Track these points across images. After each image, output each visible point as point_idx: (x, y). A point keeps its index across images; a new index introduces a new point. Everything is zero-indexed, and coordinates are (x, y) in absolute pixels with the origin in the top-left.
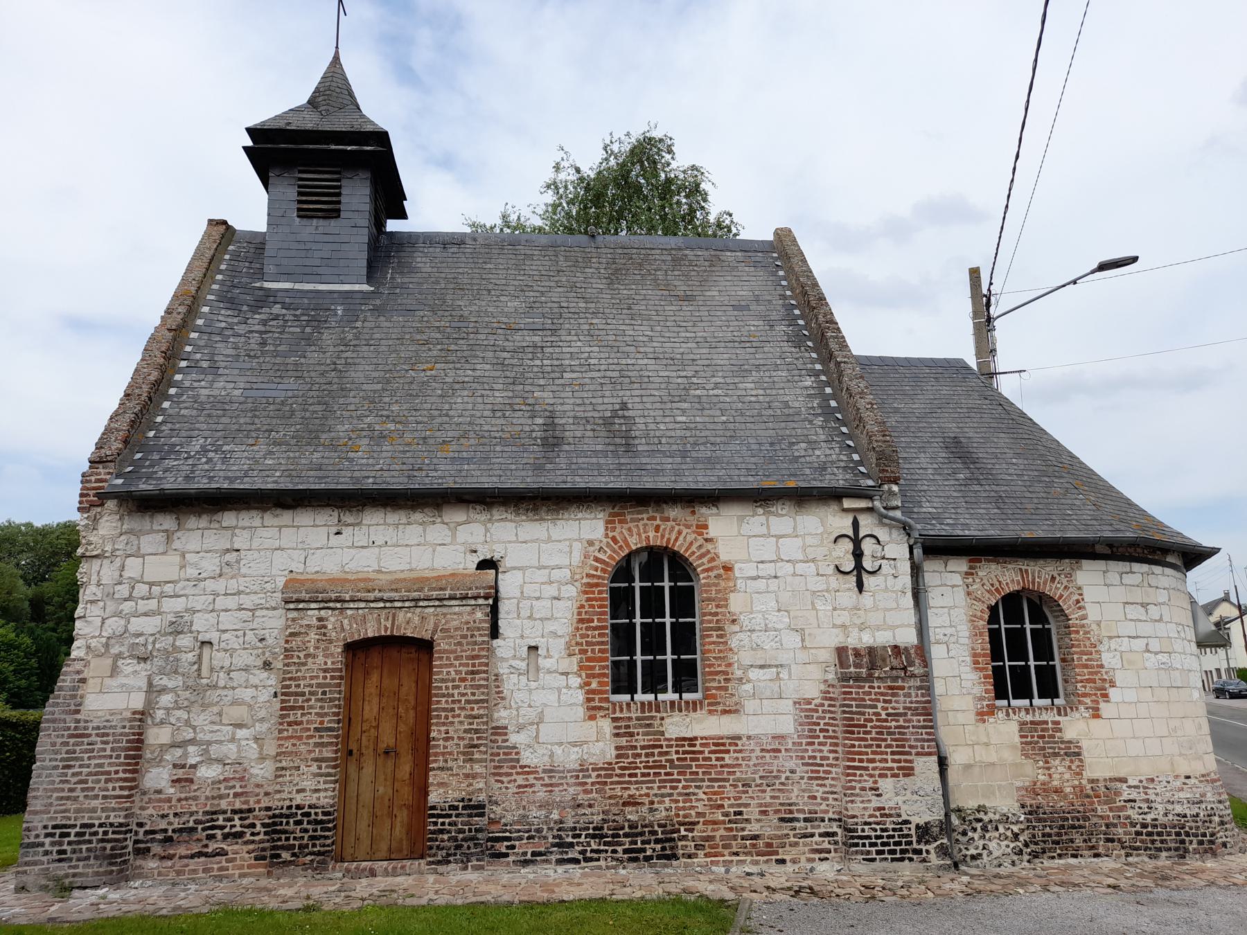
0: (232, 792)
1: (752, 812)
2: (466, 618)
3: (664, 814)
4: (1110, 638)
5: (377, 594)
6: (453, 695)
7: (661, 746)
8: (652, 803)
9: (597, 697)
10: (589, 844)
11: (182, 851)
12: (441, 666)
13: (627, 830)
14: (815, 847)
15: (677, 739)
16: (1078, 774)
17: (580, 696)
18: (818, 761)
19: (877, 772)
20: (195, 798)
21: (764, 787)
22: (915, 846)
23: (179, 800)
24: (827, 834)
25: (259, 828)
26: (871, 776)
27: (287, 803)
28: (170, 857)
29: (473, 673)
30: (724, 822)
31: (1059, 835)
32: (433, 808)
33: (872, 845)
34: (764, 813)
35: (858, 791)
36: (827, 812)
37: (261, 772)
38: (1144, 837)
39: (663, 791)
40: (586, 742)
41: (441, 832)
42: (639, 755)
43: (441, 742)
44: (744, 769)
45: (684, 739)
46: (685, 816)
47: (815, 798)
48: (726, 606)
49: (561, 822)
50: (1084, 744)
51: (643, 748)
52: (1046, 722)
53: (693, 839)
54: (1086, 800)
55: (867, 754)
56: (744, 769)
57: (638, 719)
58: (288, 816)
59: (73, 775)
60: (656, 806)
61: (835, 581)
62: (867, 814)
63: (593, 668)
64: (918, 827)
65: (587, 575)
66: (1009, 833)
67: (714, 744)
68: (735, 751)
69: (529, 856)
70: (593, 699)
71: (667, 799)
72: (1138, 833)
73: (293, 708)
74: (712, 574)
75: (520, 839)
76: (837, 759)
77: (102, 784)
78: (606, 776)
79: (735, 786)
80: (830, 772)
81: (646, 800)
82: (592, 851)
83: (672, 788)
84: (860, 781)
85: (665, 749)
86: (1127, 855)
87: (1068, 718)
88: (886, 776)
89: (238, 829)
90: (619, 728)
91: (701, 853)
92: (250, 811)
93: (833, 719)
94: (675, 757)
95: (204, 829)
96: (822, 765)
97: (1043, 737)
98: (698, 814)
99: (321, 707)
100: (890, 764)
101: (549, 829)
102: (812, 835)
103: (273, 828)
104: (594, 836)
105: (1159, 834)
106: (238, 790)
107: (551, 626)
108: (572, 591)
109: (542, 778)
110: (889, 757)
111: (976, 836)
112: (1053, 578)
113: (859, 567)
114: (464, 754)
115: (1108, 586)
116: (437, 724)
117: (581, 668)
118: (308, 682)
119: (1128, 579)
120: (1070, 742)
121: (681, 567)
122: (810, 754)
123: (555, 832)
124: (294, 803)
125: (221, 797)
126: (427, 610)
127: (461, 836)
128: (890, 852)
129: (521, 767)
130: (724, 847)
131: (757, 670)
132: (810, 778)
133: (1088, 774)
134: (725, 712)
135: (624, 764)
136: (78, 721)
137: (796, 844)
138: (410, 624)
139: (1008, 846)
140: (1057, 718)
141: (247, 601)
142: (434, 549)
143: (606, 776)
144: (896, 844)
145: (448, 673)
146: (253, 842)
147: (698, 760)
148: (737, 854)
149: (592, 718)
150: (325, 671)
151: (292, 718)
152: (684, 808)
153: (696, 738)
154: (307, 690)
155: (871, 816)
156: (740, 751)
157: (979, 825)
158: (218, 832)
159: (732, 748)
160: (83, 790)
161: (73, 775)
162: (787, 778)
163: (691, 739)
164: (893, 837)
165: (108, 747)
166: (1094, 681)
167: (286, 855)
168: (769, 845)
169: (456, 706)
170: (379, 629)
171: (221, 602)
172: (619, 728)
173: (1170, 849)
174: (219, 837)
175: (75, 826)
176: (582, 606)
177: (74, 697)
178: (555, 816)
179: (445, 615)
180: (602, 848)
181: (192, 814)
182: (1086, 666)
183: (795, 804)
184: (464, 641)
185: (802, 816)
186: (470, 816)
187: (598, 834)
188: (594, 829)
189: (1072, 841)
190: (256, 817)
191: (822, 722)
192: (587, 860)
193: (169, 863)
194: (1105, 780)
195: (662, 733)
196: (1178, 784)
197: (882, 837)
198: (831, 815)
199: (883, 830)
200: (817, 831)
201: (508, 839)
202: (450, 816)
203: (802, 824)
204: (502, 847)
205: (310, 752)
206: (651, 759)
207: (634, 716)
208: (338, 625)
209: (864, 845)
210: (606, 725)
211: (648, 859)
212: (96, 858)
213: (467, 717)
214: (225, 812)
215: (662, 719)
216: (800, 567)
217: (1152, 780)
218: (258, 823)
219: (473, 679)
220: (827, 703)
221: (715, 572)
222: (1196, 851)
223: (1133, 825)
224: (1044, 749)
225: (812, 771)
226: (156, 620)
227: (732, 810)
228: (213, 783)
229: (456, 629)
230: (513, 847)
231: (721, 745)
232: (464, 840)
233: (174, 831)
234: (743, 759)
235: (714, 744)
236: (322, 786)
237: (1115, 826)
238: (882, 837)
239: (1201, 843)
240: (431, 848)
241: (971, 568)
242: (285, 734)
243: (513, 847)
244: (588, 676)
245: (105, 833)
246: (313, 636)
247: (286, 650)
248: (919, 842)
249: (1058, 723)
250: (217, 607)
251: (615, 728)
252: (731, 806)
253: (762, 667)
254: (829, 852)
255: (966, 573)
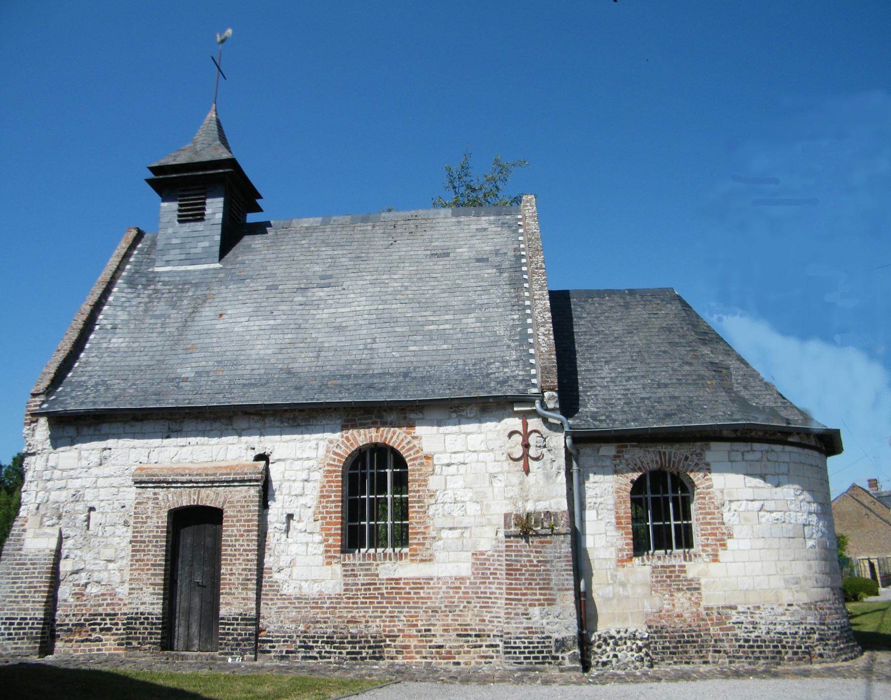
0: (105, 602)
1: (437, 630)
2: (243, 494)
3: (375, 629)
4: (730, 501)
5: (187, 478)
6: (235, 546)
7: (375, 584)
8: (367, 622)
9: (332, 549)
10: (323, 647)
11: (77, 637)
12: (228, 526)
13: (349, 639)
14: (482, 654)
15: (388, 579)
16: (696, 603)
17: (322, 548)
18: (488, 595)
19: (528, 603)
20: (85, 605)
21: (448, 613)
22: (554, 654)
23: (76, 606)
24: (492, 646)
25: (120, 626)
26: (523, 605)
27: (135, 611)
28: (71, 641)
29: (248, 531)
30: (417, 636)
31: (675, 647)
32: (223, 619)
33: (521, 653)
34: (445, 630)
35: (512, 615)
36: (492, 630)
37: (123, 591)
38: (746, 649)
39: (375, 614)
40: (323, 580)
41: (228, 634)
42: (360, 590)
43: (228, 576)
44: (433, 600)
45: (392, 579)
46: (389, 631)
47: (484, 621)
48: (426, 485)
49: (305, 632)
50: (703, 581)
51: (363, 585)
52: (674, 566)
53: (395, 647)
54: (702, 623)
55: (521, 589)
56: (433, 600)
57: (360, 565)
58: (136, 619)
59: (18, 588)
60: (370, 624)
61: (507, 465)
62: (519, 631)
63: (330, 529)
64: (557, 641)
65: (329, 465)
66: (634, 646)
67: (414, 583)
68: (428, 588)
69: (284, 654)
70: (330, 551)
71: (378, 620)
72: (740, 646)
73: (138, 551)
74: (417, 462)
75: (278, 641)
76: (501, 594)
77: (32, 594)
78: (336, 603)
79: (427, 612)
80: (496, 603)
81: (363, 620)
82: (326, 652)
83: (382, 612)
84: (514, 609)
85: (378, 586)
86: (730, 662)
87: (692, 563)
88: (535, 605)
89: (109, 626)
90: (347, 571)
91: (400, 656)
92: (115, 615)
93: (500, 565)
94: (385, 591)
95: (90, 625)
96: (490, 598)
97: (671, 577)
98: (399, 630)
99: (155, 551)
100: (538, 597)
101: (298, 636)
102: (481, 646)
103: (128, 627)
104: (327, 643)
105: (758, 647)
106: (109, 601)
107: (302, 500)
108: (318, 476)
109: (294, 603)
110: (538, 592)
111: (608, 649)
112: (687, 458)
113: (525, 456)
114: (242, 584)
115: (732, 462)
116: (225, 565)
117: (322, 529)
118: (147, 534)
119: (749, 456)
120: (692, 580)
121: (400, 461)
122: (482, 590)
123: (301, 639)
124: (139, 611)
125: (100, 605)
126: (219, 489)
127: (240, 638)
128: (535, 658)
129: (281, 595)
130: (417, 653)
131: (447, 531)
132: (481, 607)
133: (704, 603)
134: (422, 561)
135: (349, 594)
136: (21, 555)
137: (469, 652)
138: (208, 498)
139: (632, 656)
140: (684, 563)
141: (116, 481)
142: (232, 451)
143: (336, 603)
144: (539, 652)
145: (232, 531)
146: (117, 634)
147: (401, 593)
148: (425, 658)
149: (329, 564)
150: (158, 527)
151: (138, 557)
152: (389, 626)
153: (400, 579)
154: (147, 539)
155: (521, 633)
156: (432, 588)
157: (611, 642)
158: (97, 627)
159: (426, 586)
160: (22, 597)
161: (18, 588)
162: (464, 607)
163: (397, 579)
164: (537, 647)
165: (36, 571)
166: (715, 535)
167: (135, 643)
168: (450, 652)
169: (237, 553)
170: (190, 501)
171: (101, 482)
172: (347, 571)
173: (767, 658)
174: (98, 630)
175: (16, 619)
176: (324, 486)
177: (19, 540)
178: (302, 628)
179: (231, 492)
180: (332, 650)
181: (83, 615)
182: (709, 523)
183: (468, 625)
184: (242, 510)
185: (473, 633)
186: (246, 625)
187: (330, 641)
188: (327, 638)
189: (686, 652)
190: (118, 619)
191: (492, 568)
192: (322, 658)
193: (70, 644)
194: (718, 608)
195: (377, 575)
196: (781, 610)
197: (529, 648)
198: (495, 633)
199: (529, 643)
200: (484, 644)
201: (271, 641)
202: (233, 624)
203: (474, 639)
204: (267, 647)
205: (149, 579)
206: (368, 593)
207: (357, 563)
208: (165, 498)
209: (515, 653)
210: (338, 569)
211: (363, 659)
212: (28, 638)
213: (244, 560)
214: (101, 615)
215: (378, 565)
216: (482, 456)
217: (759, 608)
218: (120, 622)
219: (248, 535)
220: (496, 554)
221: (419, 461)
222: (790, 659)
223: (737, 640)
224: (670, 585)
225: (483, 602)
226: (64, 493)
227: (423, 628)
228: (95, 596)
229: (238, 502)
230: (274, 647)
231: (418, 584)
232: (242, 640)
233: (73, 625)
234: (434, 593)
235: (414, 583)
236: (155, 601)
237: (722, 641)
238: (529, 648)
239: (795, 653)
240: (221, 644)
241: (618, 452)
242: (134, 567)
243: (274, 647)
244: (327, 535)
245: (33, 624)
246: (150, 504)
247: (135, 513)
248: (557, 651)
249: (684, 566)
250: (98, 485)
251: (345, 571)
252: (423, 625)
253: (450, 529)
254: (492, 657)
255: (615, 456)
